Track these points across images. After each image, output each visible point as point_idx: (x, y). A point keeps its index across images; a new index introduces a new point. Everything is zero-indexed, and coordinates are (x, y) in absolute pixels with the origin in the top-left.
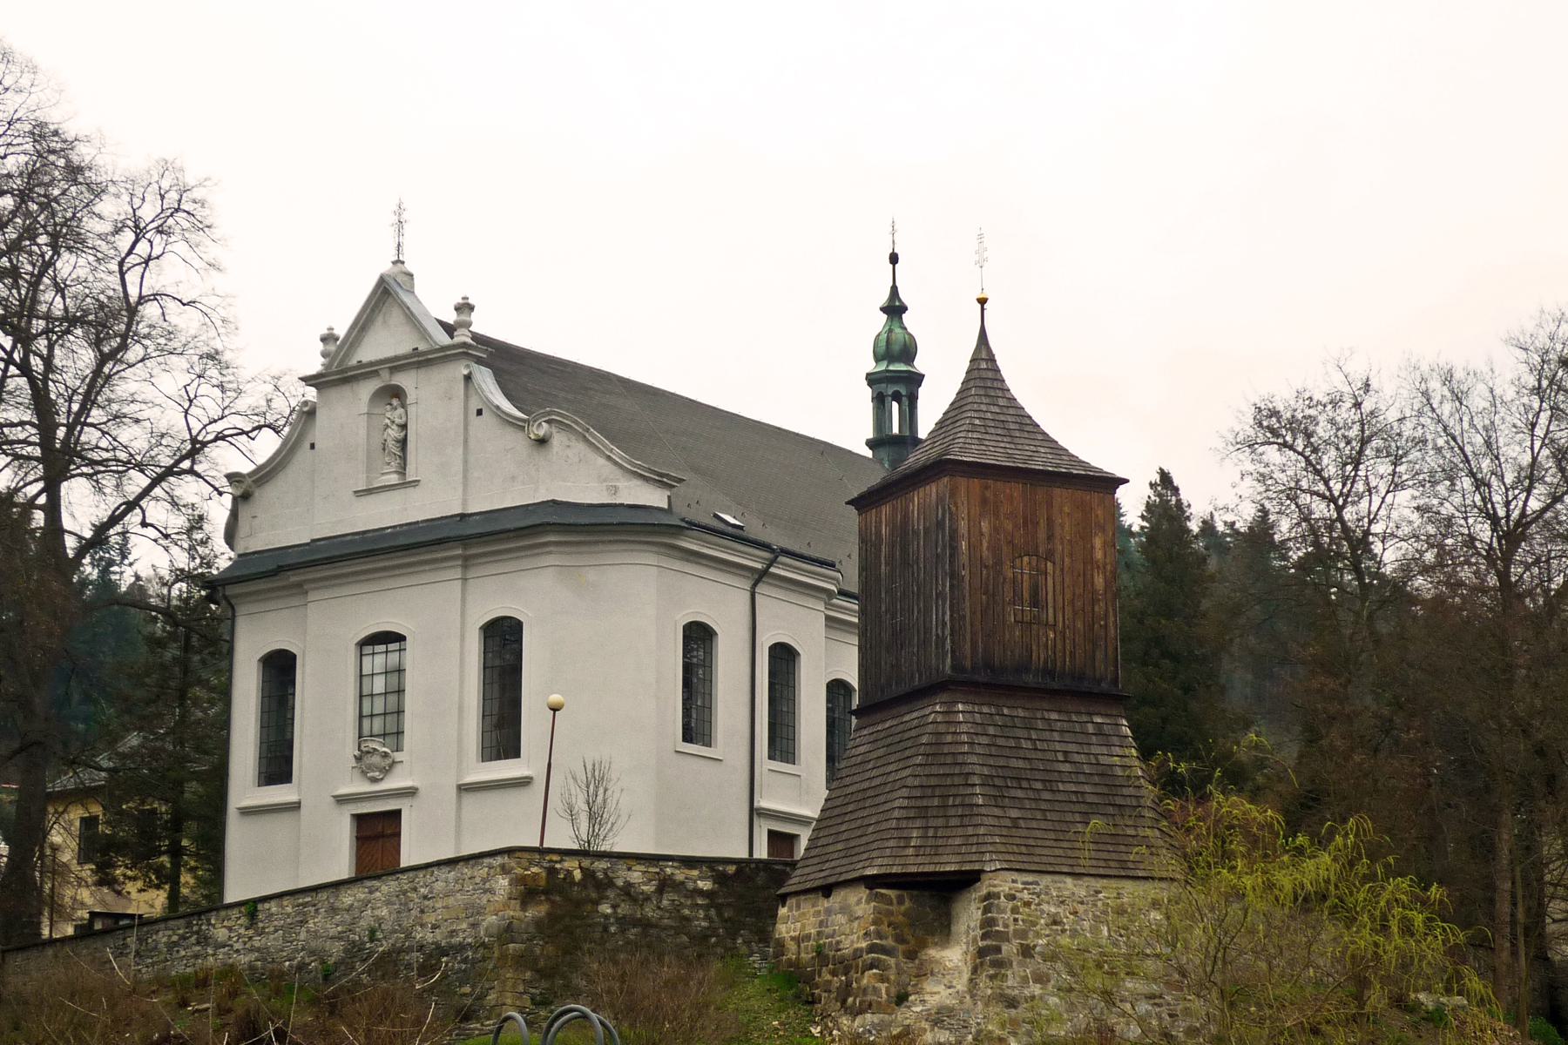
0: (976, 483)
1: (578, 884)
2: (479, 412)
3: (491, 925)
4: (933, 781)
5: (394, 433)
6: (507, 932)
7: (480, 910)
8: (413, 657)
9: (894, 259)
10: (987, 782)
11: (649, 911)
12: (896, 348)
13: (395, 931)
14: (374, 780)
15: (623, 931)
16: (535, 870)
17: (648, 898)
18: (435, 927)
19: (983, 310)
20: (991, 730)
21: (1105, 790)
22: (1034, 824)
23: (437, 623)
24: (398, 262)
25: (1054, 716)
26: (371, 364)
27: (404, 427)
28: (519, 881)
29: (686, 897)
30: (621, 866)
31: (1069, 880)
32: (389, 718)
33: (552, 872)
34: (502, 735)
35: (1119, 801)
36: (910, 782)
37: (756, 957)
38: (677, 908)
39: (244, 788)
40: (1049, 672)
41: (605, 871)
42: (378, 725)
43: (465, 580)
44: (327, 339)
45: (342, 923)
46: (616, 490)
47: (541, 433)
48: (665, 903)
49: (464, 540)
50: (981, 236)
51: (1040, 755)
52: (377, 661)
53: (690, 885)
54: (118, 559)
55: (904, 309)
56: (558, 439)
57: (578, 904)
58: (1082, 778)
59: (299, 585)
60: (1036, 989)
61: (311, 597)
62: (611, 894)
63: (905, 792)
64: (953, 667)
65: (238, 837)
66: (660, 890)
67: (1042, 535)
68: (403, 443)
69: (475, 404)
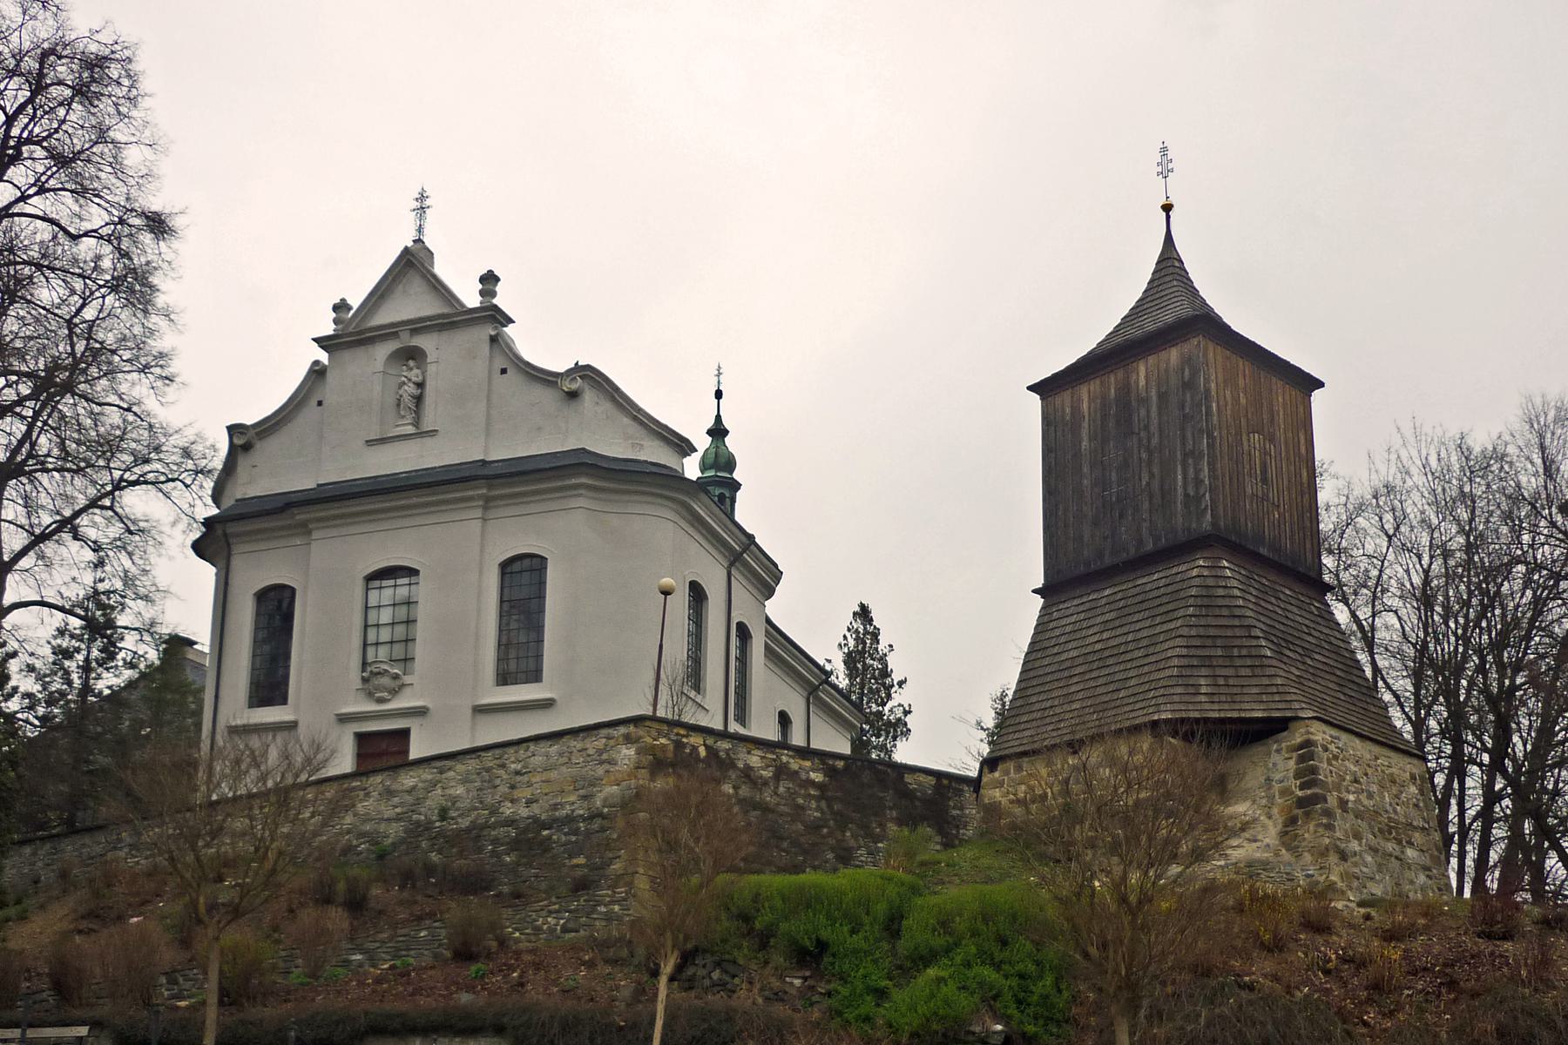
1: (702, 761)
3: (612, 795)
4: (1212, 632)
5: (410, 389)
7: (594, 782)
8: (423, 590)
9: (719, 395)
11: (767, 797)
12: (722, 460)
13: (476, 809)
14: (381, 701)
16: (663, 741)
17: (766, 783)
18: (529, 802)
19: (1168, 218)
23: (457, 563)
24: (418, 241)
26: (393, 325)
27: (420, 385)
29: (800, 786)
32: (395, 646)
33: (679, 745)
36: (1185, 632)
37: (862, 851)
38: (792, 795)
41: (727, 751)
42: (383, 652)
44: (341, 307)
45: (401, 804)
47: (574, 386)
48: (781, 789)
49: (486, 477)
50: (1164, 150)
52: (386, 593)
55: (726, 432)
61: (315, 535)
63: (1179, 641)
66: (777, 777)
68: (419, 400)
69: (500, 363)
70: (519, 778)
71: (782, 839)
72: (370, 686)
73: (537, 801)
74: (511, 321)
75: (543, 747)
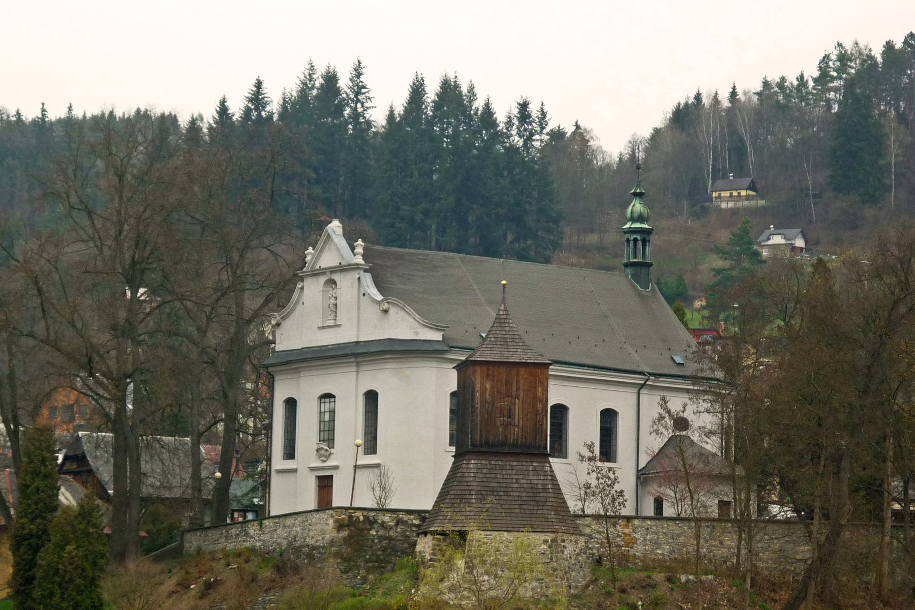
0: (485, 368)
2: (364, 295)
6: (332, 543)
10: (479, 493)
11: (392, 533)
12: (636, 215)
14: (324, 461)
15: (380, 542)
20: (485, 471)
21: (532, 494)
22: (496, 510)
25: (515, 463)
27: (336, 298)
28: (336, 521)
30: (381, 514)
31: (506, 533)
33: (350, 517)
34: (371, 446)
35: (538, 499)
38: (404, 532)
39: (278, 462)
40: (515, 445)
43: (358, 372)
46: (417, 333)
49: (355, 355)
51: (505, 481)
52: (326, 407)
53: (410, 522)
54: (538, 129)
56: (393, 310)
57: (362, 530)
58: (522, 490)
59: (295, 369)
60: (486, 578)
61: (302, 374)
62: (375, 526)
64: (472, 445)
65: (277, 483)
66: (397, 525)
67: (514, 388)
68: (336, 305)
71: (397, 551)
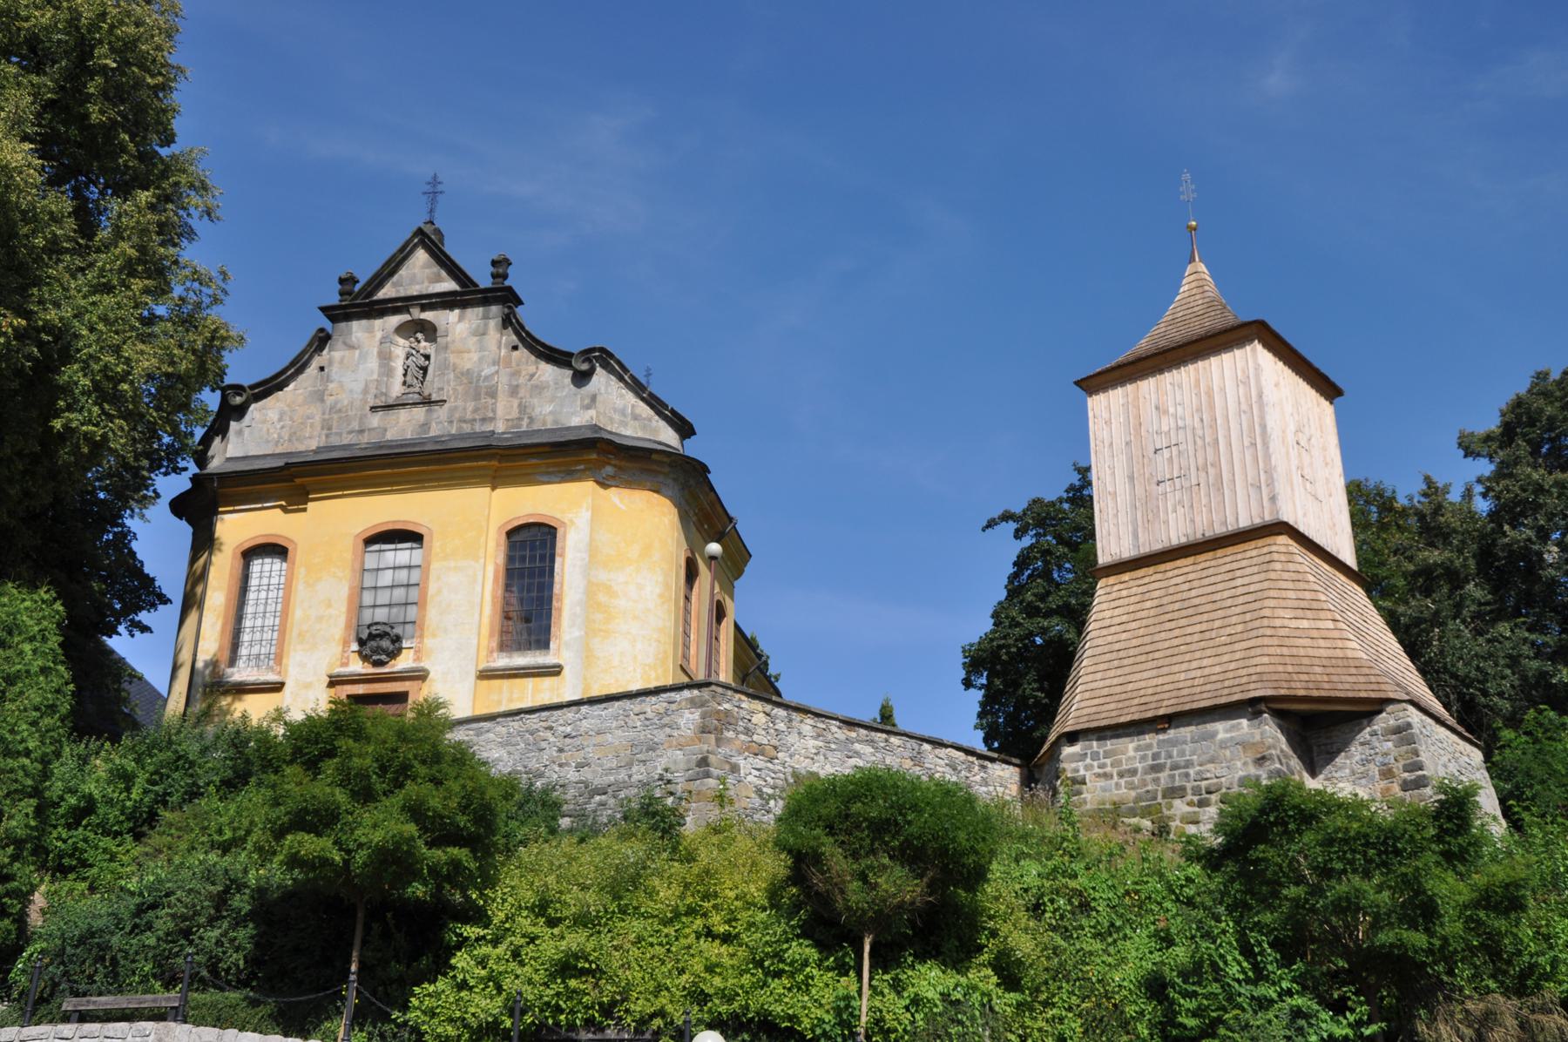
18: (579, 766)
70: (568, 741)
72: (367, 651)
73: (588, 765)
74: (520, 303)
75: (597, 710)
